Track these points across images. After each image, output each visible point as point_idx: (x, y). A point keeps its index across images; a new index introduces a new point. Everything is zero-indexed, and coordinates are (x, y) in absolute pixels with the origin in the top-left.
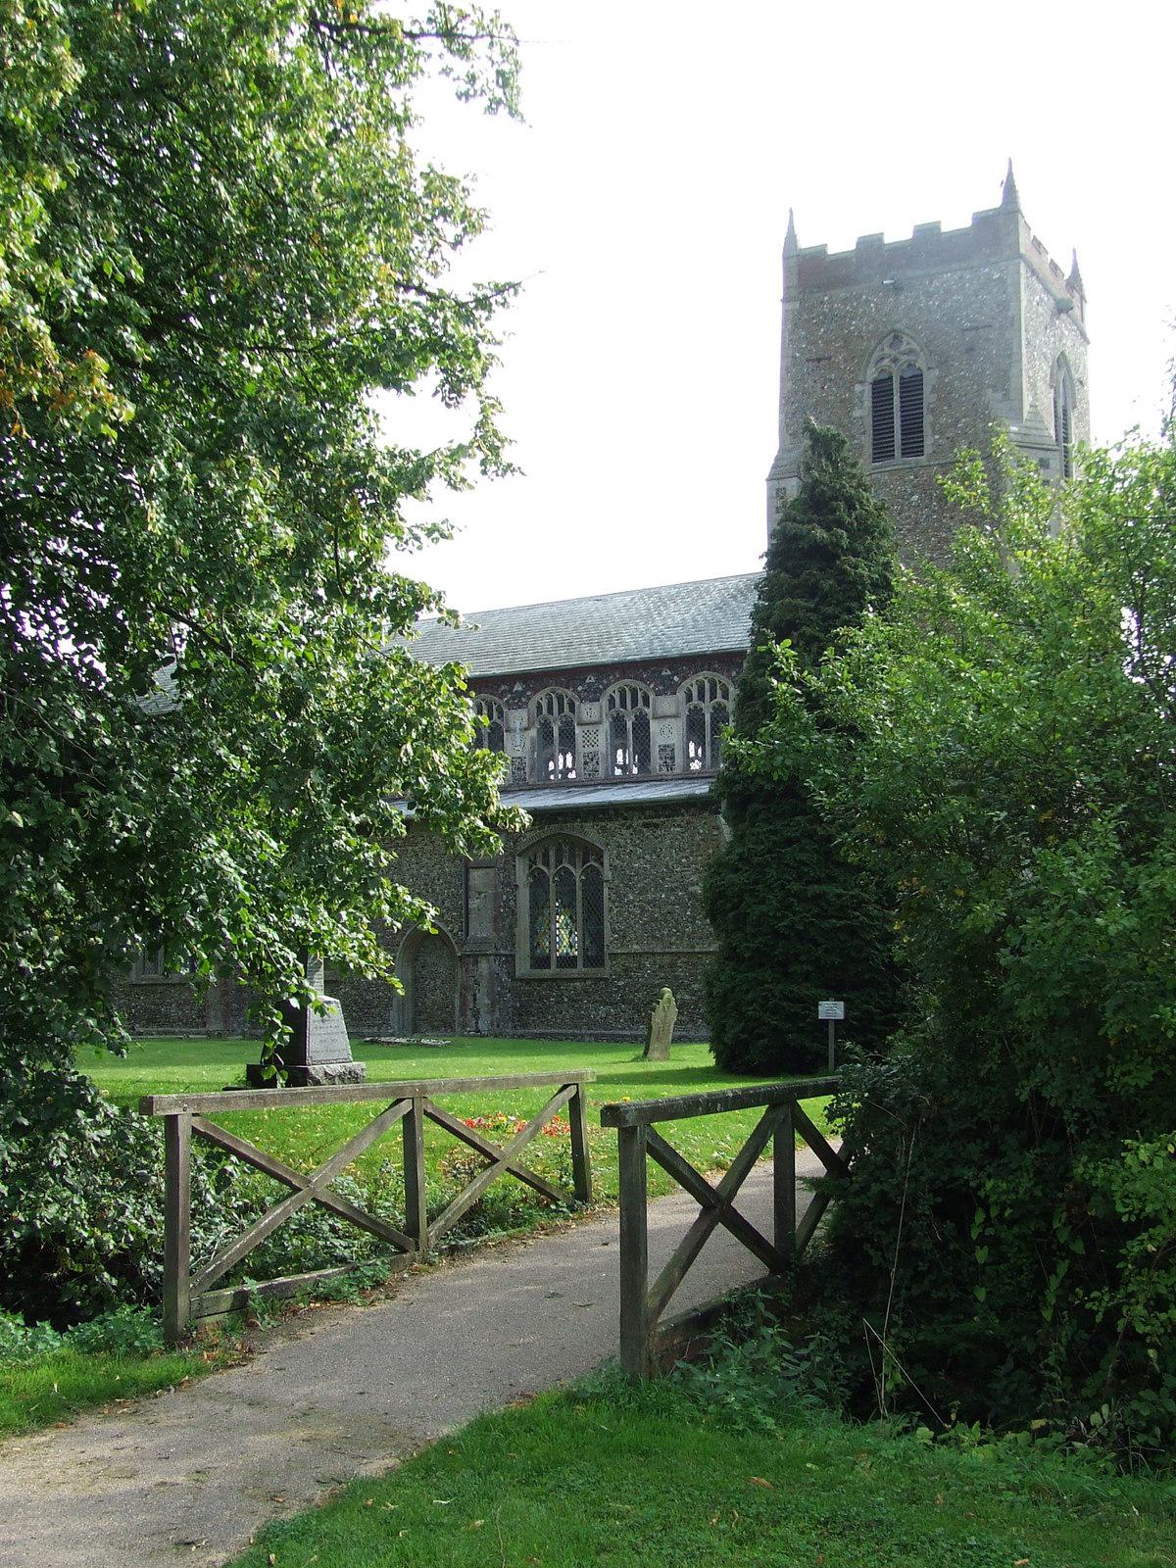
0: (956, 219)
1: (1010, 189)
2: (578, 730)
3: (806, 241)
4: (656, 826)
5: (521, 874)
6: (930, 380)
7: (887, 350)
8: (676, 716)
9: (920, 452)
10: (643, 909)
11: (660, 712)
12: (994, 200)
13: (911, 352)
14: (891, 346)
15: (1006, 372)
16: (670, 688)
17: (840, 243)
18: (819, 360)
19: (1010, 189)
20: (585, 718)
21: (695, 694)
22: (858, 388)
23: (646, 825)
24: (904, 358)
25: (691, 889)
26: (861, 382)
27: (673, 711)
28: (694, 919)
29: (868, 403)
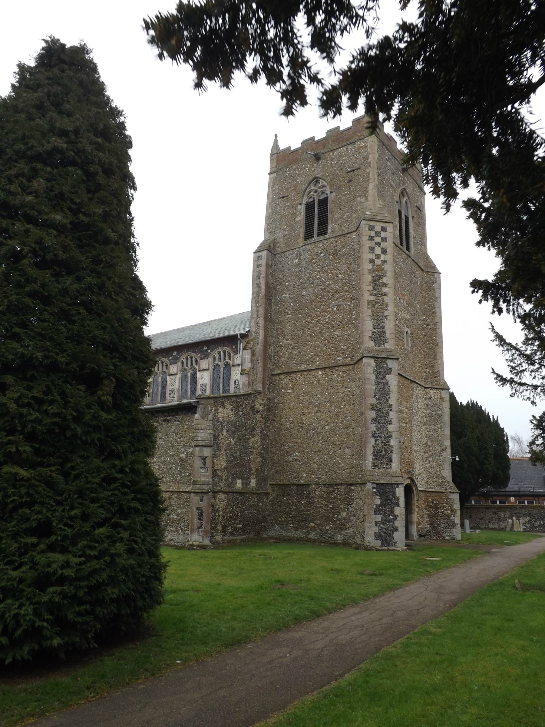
2: (168, 378)
3: (282, 146)
4: (168, 421)
6: (331, 197)
7: (313, 188)
9: (326, 233)
10: (159, 466)
11: (202, 368)
13: (323, 186)
14: (315, 185)
15: (366, 188)
16: (206, 356)
17: (295, 145)
18: (283, 197)
20: (172, 372)
21: (217, 358)
22: (299, 207)
23: (164, 421)
24: (320, 190)
25: (181, 456)
26: (300, 204)
27: (207, 367)
28: (181, 472)
29: (303, 214)
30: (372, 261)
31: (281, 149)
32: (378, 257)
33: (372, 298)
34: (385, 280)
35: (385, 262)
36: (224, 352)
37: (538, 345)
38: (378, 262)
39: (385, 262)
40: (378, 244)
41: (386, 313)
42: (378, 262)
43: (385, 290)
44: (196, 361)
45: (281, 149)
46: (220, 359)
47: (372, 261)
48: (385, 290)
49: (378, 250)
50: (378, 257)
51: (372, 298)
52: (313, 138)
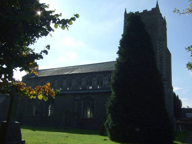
0: (149, 9)
1: (157, 5)
2: (92, 82)
3: (128, 12)
5: (82, 102)
8: (107, 80)
12: (154, 6)
19: (157, 5)
30: (160, 53)
31: (127, 13)
32: (161, 52)
33: (160, 63)
34: (163, 58)
35: (163, 53)
36: (90, 77)
37: (53, 98)
38: (161, 53)
39: (163, 53)
40: (161, 48)
41: (163, 68)
42: (161, 53)
43: (163, 61)
44: (91, 77)
45: (127, 13)
46: (99, 78)
47: (160, 53)
48: (163, 61)
49: (161, 50)
50: (161, 52)
51: (160, 63)
52: (138, 12)
